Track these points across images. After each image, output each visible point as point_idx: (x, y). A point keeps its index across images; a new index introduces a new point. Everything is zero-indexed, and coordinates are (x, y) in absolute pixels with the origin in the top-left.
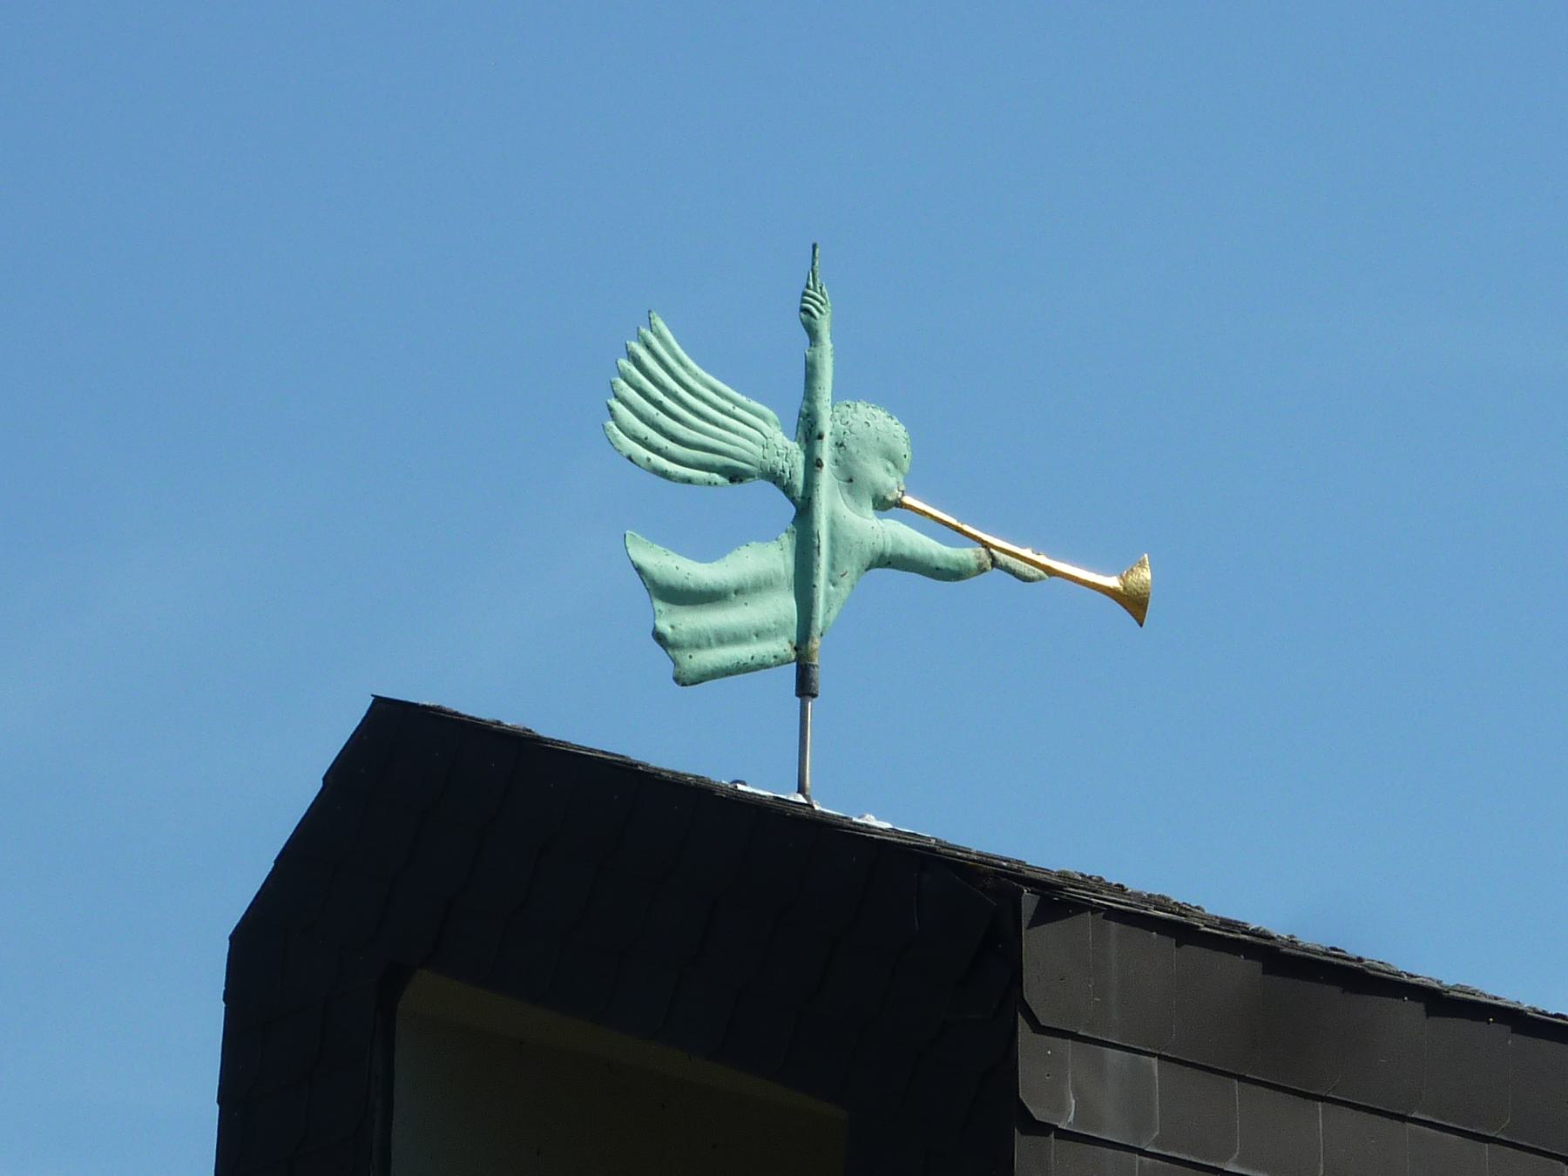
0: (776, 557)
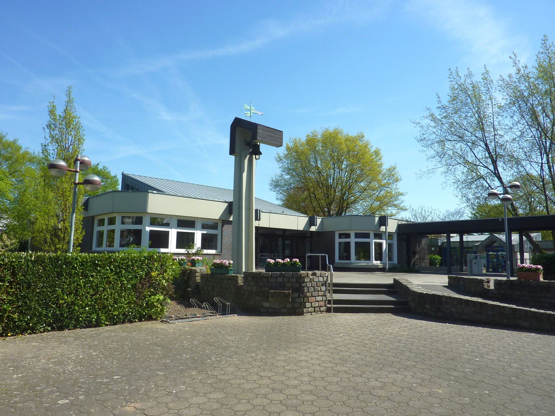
0: (250, 112)
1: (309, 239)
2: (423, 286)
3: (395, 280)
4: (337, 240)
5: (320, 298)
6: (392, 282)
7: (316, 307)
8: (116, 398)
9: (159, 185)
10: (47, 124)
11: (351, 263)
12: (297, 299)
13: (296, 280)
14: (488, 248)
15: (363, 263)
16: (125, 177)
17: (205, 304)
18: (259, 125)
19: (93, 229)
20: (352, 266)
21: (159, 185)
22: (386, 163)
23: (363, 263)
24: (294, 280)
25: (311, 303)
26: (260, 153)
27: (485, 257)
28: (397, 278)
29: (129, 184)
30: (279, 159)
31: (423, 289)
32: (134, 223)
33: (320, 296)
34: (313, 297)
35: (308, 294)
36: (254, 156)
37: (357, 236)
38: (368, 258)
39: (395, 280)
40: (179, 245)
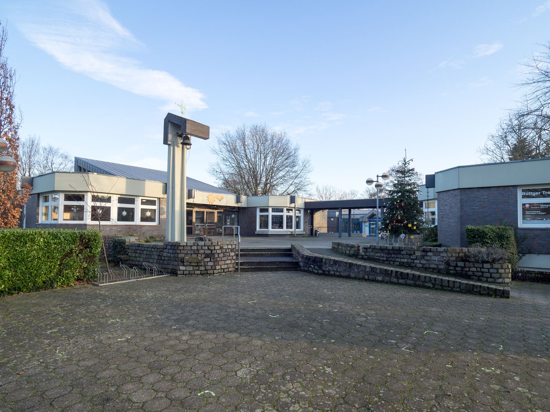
1: (237, 213)
2: (311, 250)
3: (292, 246)
4: (258, 214)
5: (229, 262)
6: (289, 246)
7: (225, 268)
8: (214, 325)
9: (109, 168)
10: (415, 171)
11: (269, 231)
12: (209, 263)
13: (208, 248)
14: (370, 219)
15: (278, 231)
16: (77, 160)
17: (135, 269)
18: (188, 120)
19: (39, 204)
20: (269, 233)
21: (109, 168)
22: (301, 156)
23: (278, 231)
24: (206, 248)
25: (221, 265)
26: (190, 144)
27: (367, 225)
28: (293, 244)
29: (81, 166)
30: (214, 151)
31: (310, 253)
32: (422, 206)
33: (229, 260)
34: (223, 261)
35: (218, 259)
36: (185, 146)
37: (274, 210)
38: (281, 226)
39: (292, 246)
40: (94, 217)
